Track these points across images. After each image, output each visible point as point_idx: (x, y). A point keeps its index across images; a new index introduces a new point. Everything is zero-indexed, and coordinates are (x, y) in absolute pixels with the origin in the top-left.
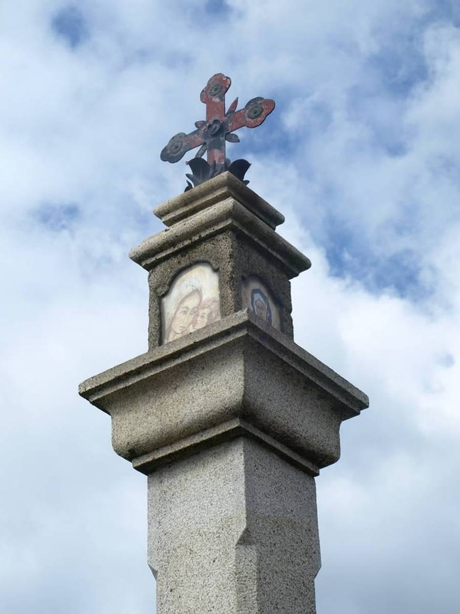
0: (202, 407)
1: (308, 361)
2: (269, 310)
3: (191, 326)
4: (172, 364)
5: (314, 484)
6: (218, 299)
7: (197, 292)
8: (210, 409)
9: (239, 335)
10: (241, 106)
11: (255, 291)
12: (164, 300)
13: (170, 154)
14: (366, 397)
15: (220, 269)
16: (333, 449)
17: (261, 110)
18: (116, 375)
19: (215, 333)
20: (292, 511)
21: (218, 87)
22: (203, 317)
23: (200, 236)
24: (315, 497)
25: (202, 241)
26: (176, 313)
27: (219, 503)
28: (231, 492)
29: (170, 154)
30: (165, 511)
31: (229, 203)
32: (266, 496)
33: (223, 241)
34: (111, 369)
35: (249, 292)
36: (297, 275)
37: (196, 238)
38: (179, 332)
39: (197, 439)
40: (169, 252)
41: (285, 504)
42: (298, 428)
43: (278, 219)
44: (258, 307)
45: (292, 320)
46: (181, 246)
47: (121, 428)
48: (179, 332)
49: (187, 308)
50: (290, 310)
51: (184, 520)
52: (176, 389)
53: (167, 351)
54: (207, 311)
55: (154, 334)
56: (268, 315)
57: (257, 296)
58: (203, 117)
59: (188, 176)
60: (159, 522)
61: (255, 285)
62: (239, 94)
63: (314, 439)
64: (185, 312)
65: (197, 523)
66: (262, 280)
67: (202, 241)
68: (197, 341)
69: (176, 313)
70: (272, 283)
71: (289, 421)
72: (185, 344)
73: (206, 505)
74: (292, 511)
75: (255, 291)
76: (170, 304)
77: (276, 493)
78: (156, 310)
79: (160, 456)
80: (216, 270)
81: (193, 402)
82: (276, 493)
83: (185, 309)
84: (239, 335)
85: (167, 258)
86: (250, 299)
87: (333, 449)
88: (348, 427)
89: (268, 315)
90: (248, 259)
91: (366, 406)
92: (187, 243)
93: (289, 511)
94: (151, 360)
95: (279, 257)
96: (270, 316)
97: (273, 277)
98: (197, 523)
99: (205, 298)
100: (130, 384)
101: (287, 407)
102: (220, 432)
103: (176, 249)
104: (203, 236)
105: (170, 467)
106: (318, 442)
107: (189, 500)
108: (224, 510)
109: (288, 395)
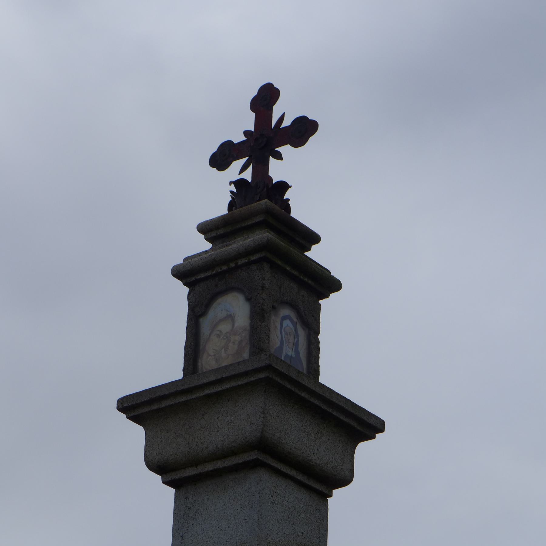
0: (225, 437)
1: (327, 395)
2: (296, 335)
3: (223, 350)
4: (201, 394)
5: (326, 505)
6: (248, 328)
7: (230, 317)
8: (232, 440)
9: (262, 375)
10: (287, 123)
11: (284, 318)
12: (201, 320)
13: (221, 159)
14: (382, 423)
15: (252, 299)
16: (347, 473)
17: (302, 130)
18: (151, 396)
19: (240, 372)
20: (303, 534)
21: (266, 97)
22: (234, 343)
23: (236, 264)
24: (327, 517)
25: (238, 267)
26: (210, 335)
27: (235, 527)
28: (246, 518)
29: (221, 159)
30: (188, 527)
31: (262, 236)
32: (278, 522)
33: (258, 272)
34: (206, 251)
35: (279, 320)
36: (327, 296)
37: (232, 265)
38: (212, 354)
39: (220, 464)
40: (208, 274)
41: (296, 528)
42: (313, 457)
43: (313, 238)
44: (286, 334)
45: (319, 342)
46: (218, 270)
47: (153, 445)
48: (212, 354)
49: (221, 332)
50: (318, 332)
51: (204, 538)
52: (203, 415)
53: (197, 381)
54: (237, 338)
55: (189, 353)
56: (296, 339)
57: (287, 323)
58: (251, 127)
59: (231, 192)
60: (182, 537)
61: (286, 311)
62: (285, 111)
63: (329, 465)
64: (219, 336)
65: (215, 543)
66: (293, 306)
67: (238, 267)
68: (224, 376)
69: (210, 335)
70: (302, 308)
71: (304, 451)
72: (213, 378)
73: (224, 526)
74: (303, 534)
75: (284, 318)
76: (206, 324)
77: (289, 517)
78: (192, 330)
79: (186, 475)
80: (248, 299)
81: (218, 431)
82: (289, 517)
83: (218, 333)
84: (262, 375)
85: (206, 279)
86: (278, 326)
87: (347, 473)
88: (363, 450)
89: (296, 339)
90: (280, 288)
91: (382, 430)
92: (224, 268)
93: (299, 534)
94: (183, 388)
95: (310, 282)
96: (298, 341)
97: (303, 302)
98: (215, 543)
99: (237, 325)
100: (163, 406)
101: (304, 437)
102: (240, 461)
103: (214, 272)
104: (239, 264)
105: (195, 485)
106: (333, 467)
107: (209, 519)
108: (239, 534)
109: (305, 426)
